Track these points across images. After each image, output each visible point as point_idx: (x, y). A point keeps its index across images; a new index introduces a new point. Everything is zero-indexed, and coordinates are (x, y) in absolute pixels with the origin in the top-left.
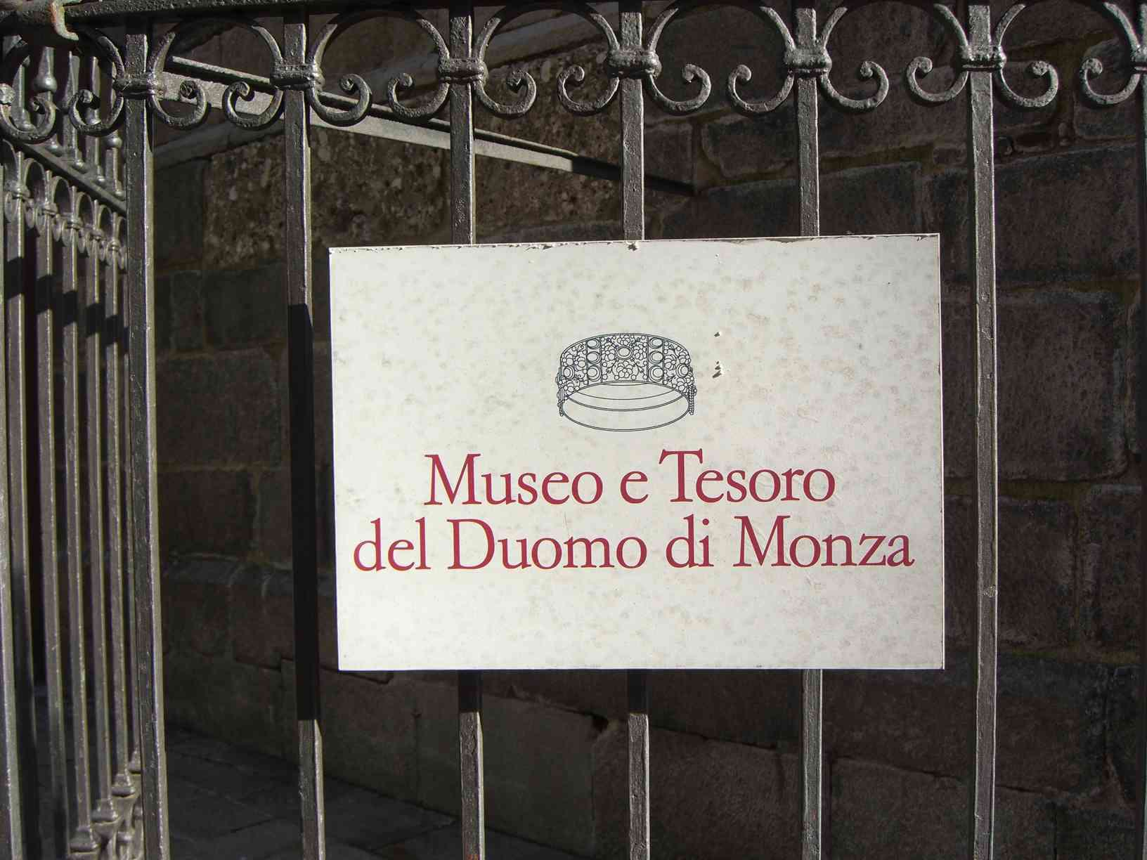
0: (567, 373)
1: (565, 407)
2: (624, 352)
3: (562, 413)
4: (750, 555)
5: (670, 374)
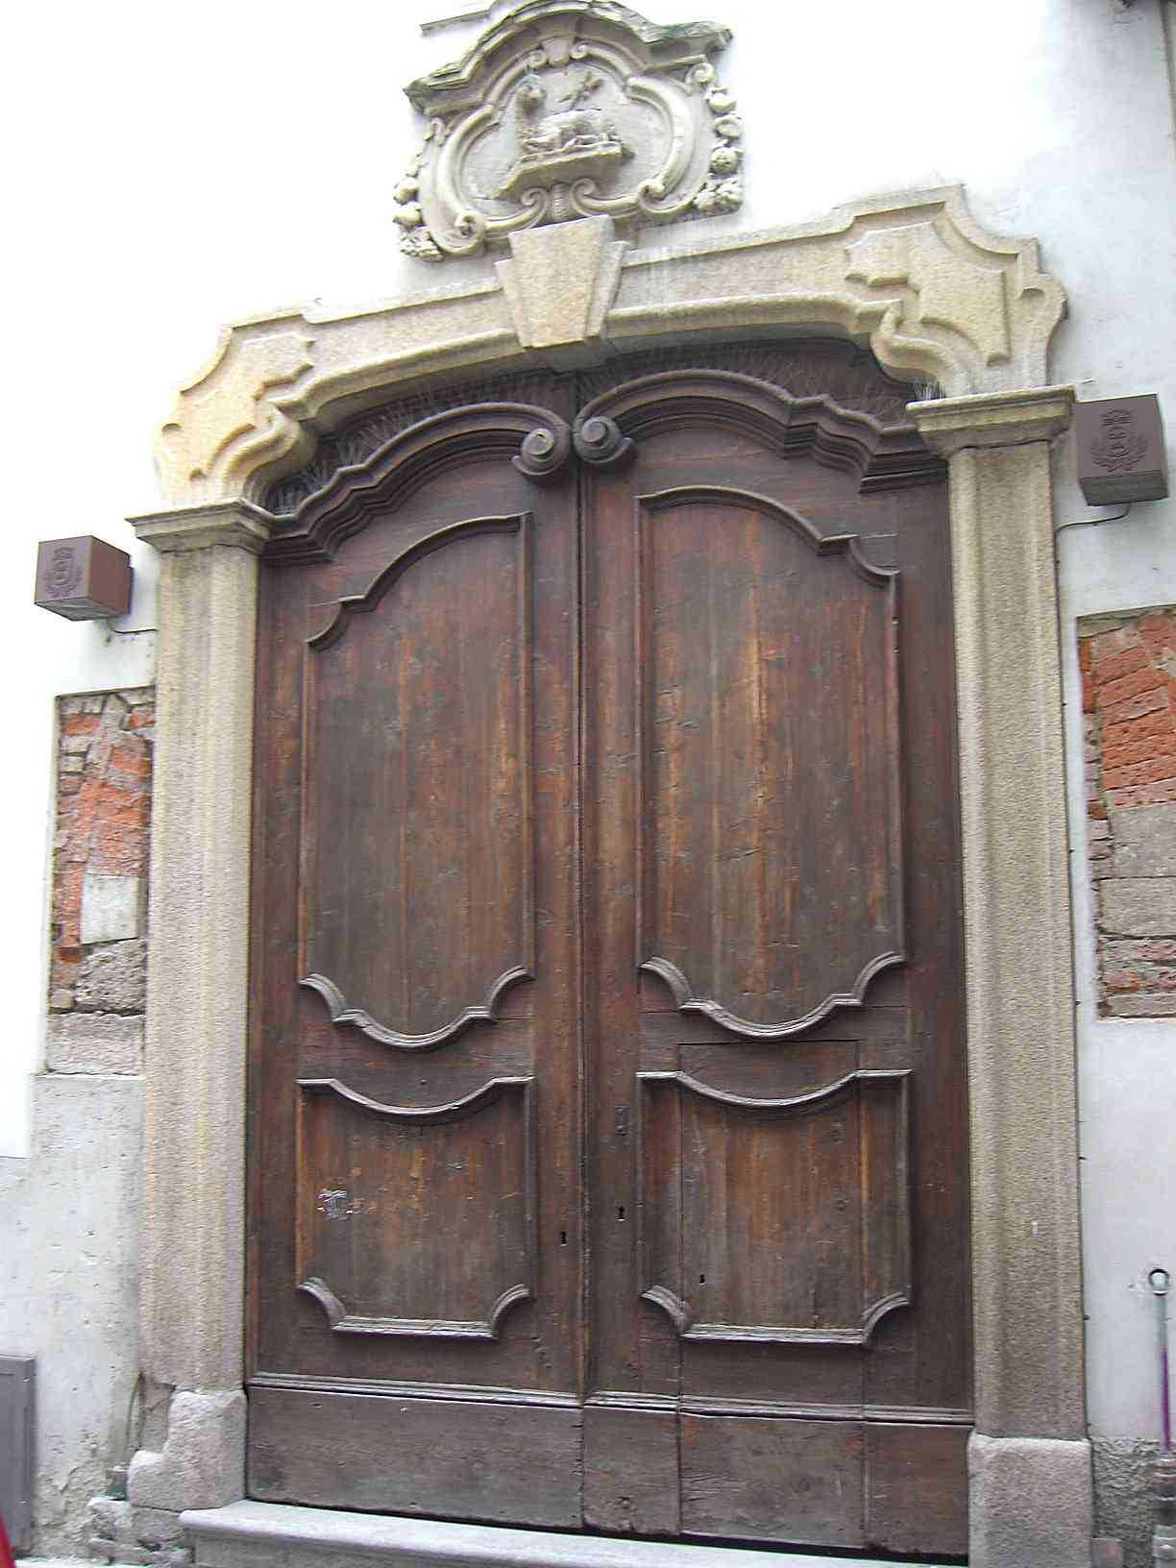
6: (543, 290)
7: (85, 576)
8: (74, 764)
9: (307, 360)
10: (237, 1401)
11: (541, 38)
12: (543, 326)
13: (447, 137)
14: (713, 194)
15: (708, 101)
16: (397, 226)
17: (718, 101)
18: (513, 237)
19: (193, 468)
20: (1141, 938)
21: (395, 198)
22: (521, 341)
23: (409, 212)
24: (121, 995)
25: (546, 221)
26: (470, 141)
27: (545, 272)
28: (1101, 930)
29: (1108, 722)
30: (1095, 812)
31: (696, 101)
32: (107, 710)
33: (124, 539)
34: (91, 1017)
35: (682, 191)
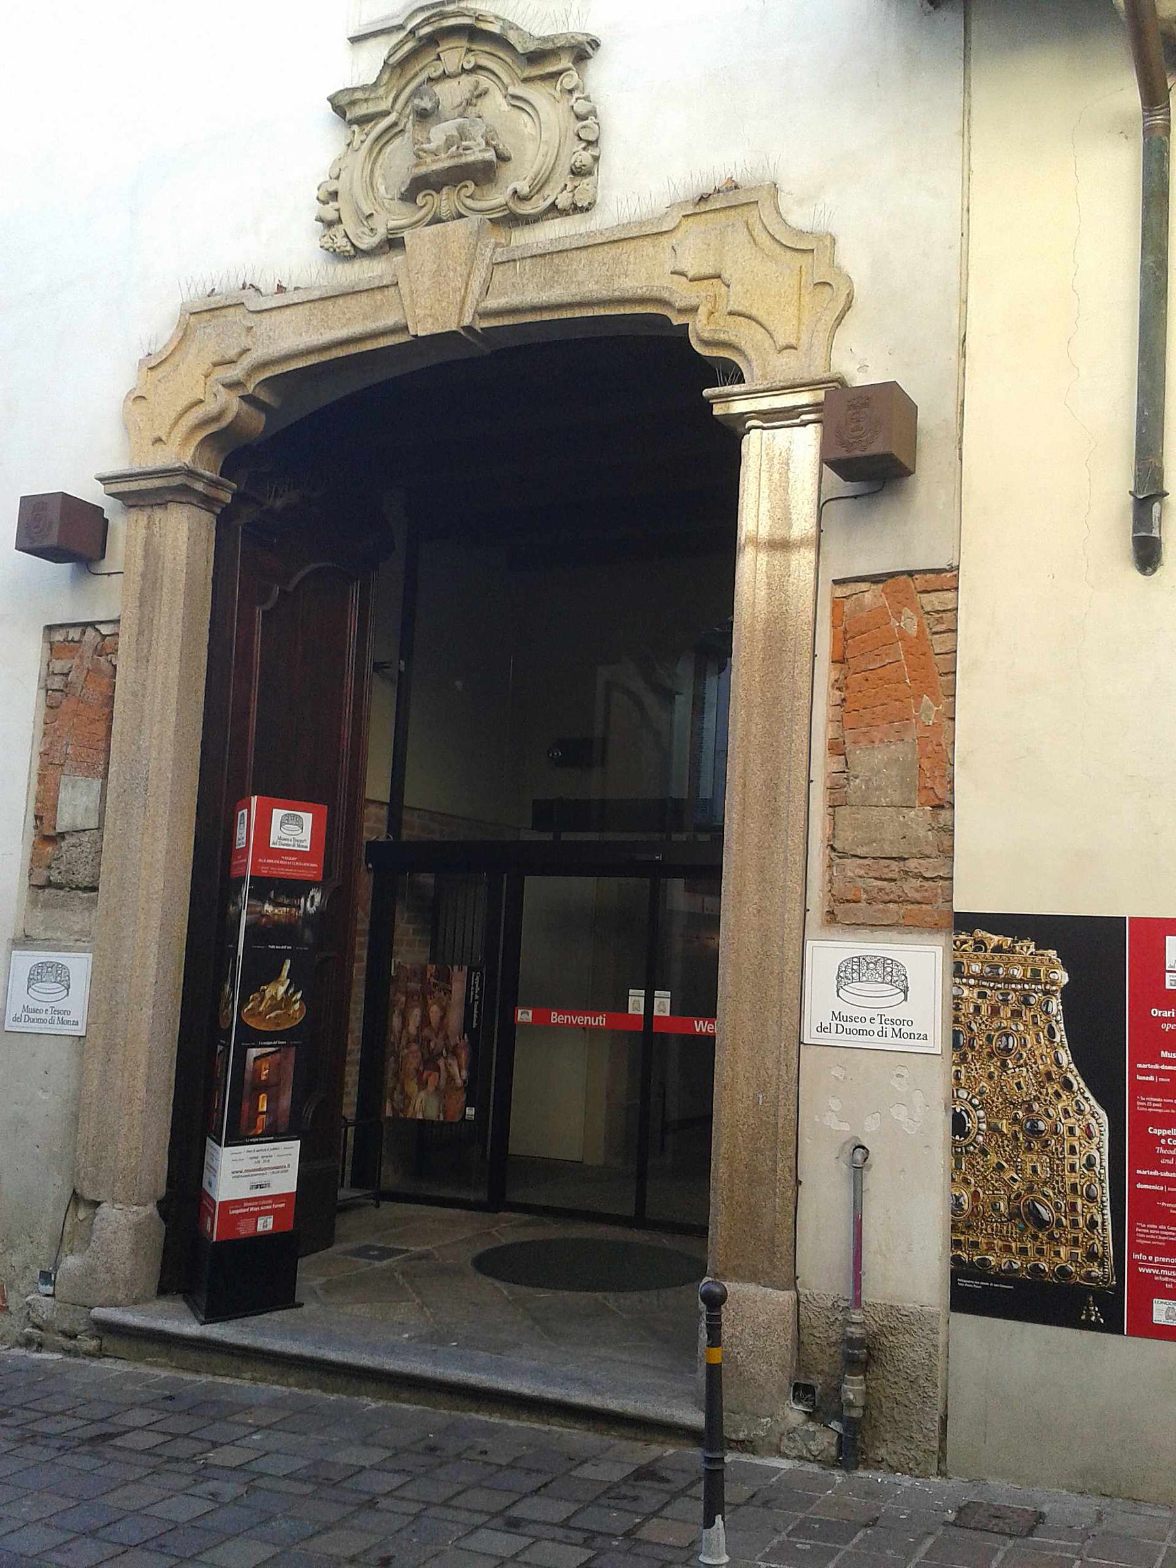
0: (842, 975)
1: (840, 992)
2: (872, 965)
3: (838, 996)
4: (894, 1035)
5: (896, 979)
6: (428, 283)
7: (56, 528)
8: (57, 683)
9: (247, 342)
10: (150, 1217)
11: (439, 50)
12: (425, 316)
13: (362, 142)
14: (571, 195)
15: (572, 107)
16: (320, 224)
17: (581, 107)
18: (406, 234)
19: (155, 435)
20: (866, 858)
21: (318, 199)
22: (410, 330)
23: (329, 212)
24: (82, 876)
25: (437, 220)
26: (379, 147)
27: (430, 267)
28: (833, 849)
29: (852, 671)
30: (836, 748)
31: (563, 106)
32: (86, 638)
33: (93, 493)
34: (62, 893)
35: (546, 191)
